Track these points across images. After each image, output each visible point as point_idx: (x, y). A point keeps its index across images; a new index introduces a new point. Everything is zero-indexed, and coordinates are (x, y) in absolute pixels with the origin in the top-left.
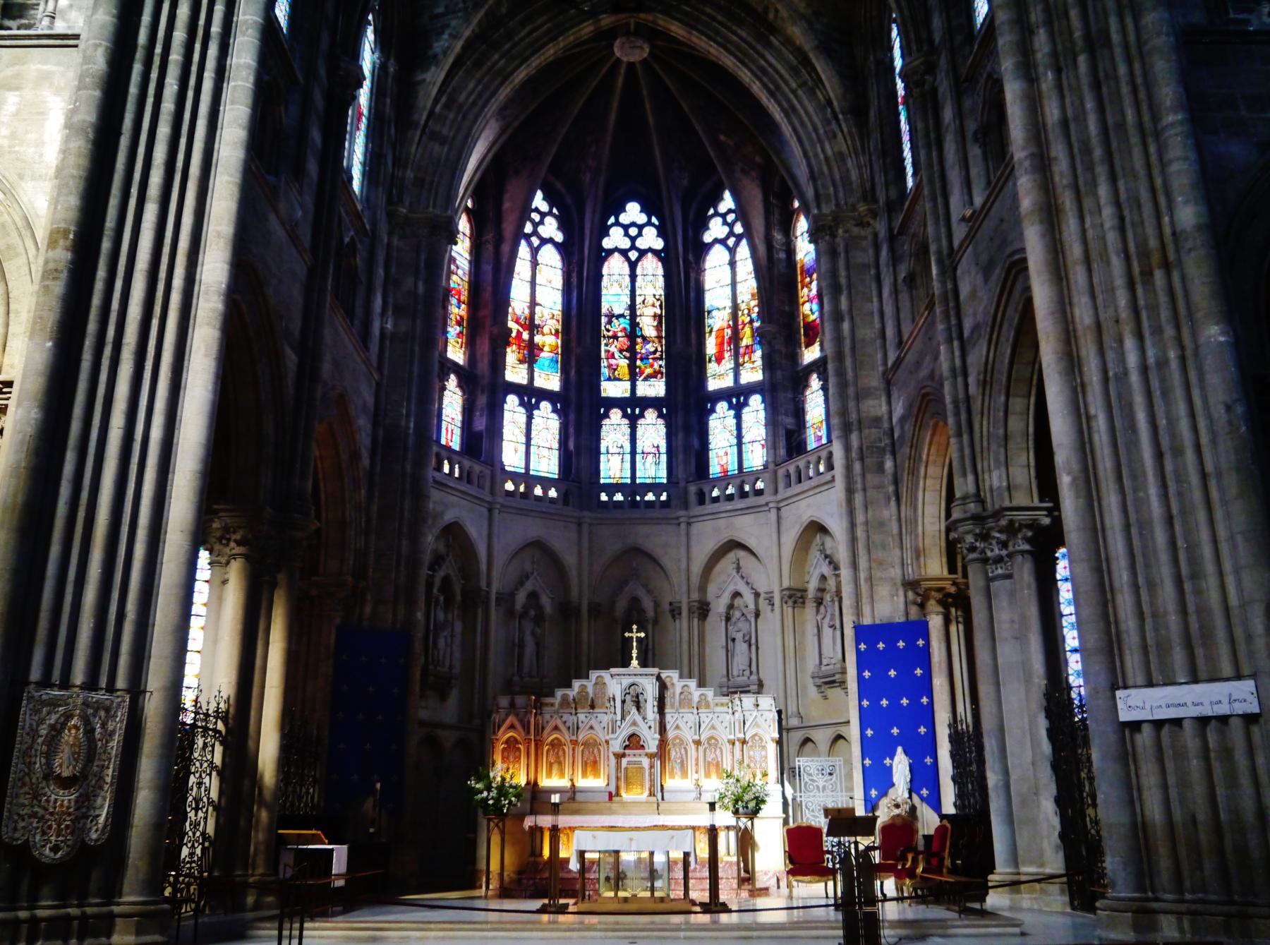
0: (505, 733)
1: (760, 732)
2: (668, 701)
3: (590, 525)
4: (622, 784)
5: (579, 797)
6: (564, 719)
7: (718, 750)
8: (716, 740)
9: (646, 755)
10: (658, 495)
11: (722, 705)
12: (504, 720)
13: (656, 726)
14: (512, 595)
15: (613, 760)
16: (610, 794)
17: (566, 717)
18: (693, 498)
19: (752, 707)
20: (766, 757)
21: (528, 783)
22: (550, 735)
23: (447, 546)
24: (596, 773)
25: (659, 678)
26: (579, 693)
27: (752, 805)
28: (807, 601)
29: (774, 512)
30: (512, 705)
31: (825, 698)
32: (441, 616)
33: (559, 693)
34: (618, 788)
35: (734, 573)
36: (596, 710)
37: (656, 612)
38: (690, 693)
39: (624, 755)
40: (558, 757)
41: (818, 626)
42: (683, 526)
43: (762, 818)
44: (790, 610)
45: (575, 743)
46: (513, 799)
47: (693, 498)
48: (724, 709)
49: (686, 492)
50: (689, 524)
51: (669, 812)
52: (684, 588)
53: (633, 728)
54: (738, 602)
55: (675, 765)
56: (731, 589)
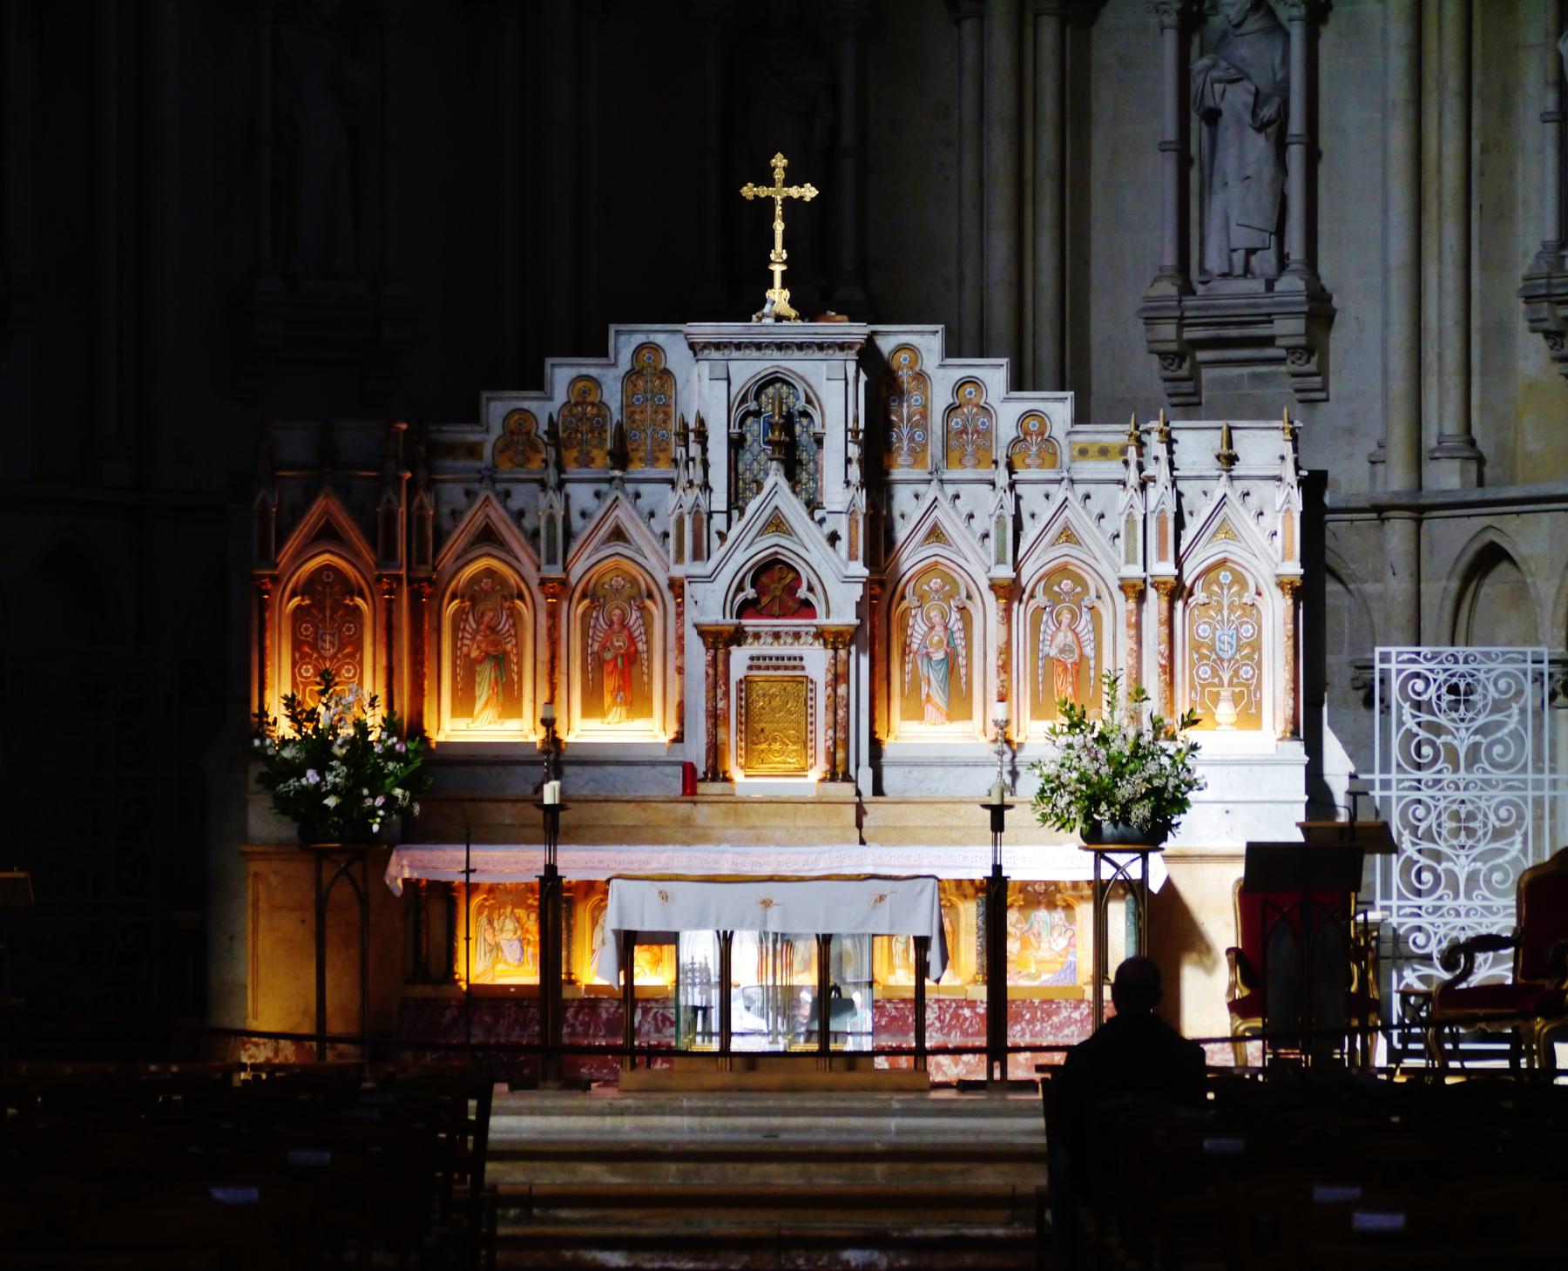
0: (300, 557)
1: (1235, 552)
2: (902, 437)
4: (732, 737)
6: (516, 503)
7: (1086, 617)
8: (1079, 581)
9: (820, 634)
11: (1104, 452)
12: (298, 512)
17: (522, 496)
19: (1210, 465)
20: (1256, 646)
22: (463, 559)
24: (635, 697)
25: (869, 356)
27: (1141, 812)
33: (497, 409)
34: (715, 751)
36: (638, 470)
38: (985, 410)
43: (1231, 857)
45: (559, 589)
46: (398, 792)
48: (1113, 468)
51: (903, 836)
53: (771, 540)
55: (923, 669)
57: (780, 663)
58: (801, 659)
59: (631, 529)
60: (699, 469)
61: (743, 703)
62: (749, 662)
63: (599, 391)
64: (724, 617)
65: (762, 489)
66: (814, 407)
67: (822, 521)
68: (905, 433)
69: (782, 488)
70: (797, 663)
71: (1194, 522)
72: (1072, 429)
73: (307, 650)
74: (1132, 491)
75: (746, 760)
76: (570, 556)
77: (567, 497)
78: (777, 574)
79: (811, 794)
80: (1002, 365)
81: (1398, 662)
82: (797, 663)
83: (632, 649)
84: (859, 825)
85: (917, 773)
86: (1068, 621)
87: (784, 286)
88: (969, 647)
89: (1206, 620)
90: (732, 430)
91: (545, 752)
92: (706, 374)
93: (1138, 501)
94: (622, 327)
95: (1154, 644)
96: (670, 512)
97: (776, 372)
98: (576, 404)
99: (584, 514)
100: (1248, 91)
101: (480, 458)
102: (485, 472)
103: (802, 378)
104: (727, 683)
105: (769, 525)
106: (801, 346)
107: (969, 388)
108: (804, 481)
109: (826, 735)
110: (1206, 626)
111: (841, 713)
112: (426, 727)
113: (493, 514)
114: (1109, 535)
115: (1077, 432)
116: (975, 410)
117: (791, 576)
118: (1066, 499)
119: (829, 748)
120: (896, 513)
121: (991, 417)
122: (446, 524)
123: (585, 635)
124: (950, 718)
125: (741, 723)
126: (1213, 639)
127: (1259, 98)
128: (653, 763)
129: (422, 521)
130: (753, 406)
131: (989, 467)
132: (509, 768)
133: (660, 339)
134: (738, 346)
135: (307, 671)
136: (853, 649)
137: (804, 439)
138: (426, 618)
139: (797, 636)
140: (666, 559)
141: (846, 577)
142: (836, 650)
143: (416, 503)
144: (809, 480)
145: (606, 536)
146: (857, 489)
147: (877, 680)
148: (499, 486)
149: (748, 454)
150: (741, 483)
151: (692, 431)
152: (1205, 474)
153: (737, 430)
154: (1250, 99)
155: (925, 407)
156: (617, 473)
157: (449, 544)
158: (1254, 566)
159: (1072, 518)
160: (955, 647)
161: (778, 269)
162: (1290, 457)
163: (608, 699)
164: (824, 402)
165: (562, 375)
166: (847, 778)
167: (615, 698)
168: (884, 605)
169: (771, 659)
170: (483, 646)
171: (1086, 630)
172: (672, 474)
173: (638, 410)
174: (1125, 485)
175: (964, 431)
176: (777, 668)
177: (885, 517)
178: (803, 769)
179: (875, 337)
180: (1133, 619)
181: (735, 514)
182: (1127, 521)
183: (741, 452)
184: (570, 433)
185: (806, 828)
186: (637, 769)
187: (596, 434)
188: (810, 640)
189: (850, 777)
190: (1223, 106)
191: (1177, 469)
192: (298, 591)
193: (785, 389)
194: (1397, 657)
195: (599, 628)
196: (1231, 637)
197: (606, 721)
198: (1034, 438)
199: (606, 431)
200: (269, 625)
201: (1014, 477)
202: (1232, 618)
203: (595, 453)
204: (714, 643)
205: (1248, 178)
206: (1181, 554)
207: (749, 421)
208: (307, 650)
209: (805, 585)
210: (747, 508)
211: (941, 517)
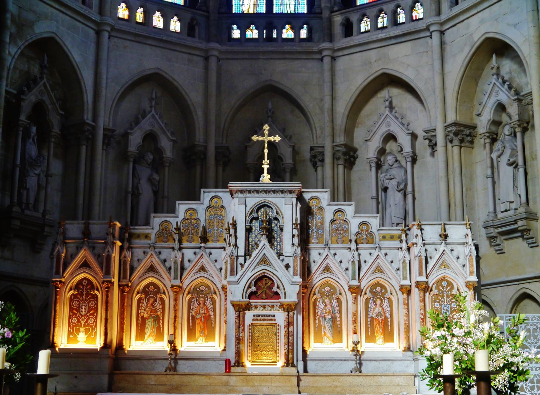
0: (73, 274)
1: (449, 274)
3: (219, 60)
4: (245, 348)
5: (183, 367)
6: (163, 257)
9: (282, 306)
10: (297, 30)
11: (392, 237)
12: (73, 257)
13: (295, 264)
14: (126, 135)
15: (232, 314)
16: (228, 362)
17: (165, 254)
18: (338, 29)
19: (437, 239)
21: (106, 345)
22: (142, 278)
23: (42, 67)
24: (209, 333)
26: (184, 219)
28: (476, 141)
29: (436, 36)
30: (86, 233)
31: (501, 252)
32: (33, 150)
33: (157, 220)
35: (387, 112)
36: (209, 244)
37: (294, 159)
39: (248, 307)
40: (154, 310)
41: (492, 167)
42: (327, 60)
44: (456, 150)
45: (178, 290)
47: (338, 29)
49: (330, 21)
50: (333, 59)
52: (328, 130)
54: (391, 146)
55: (323, 322)
56: (383, 130)
57: (266, 318)
58: (274, 316)
59: (208, 267)
60: (233, 239)
61: (250, 334)
62: (253, 318)
63: (197, 214)
64: (243, 299)
65: (258, 247)
66: (279, 216)
67: (283, 260)
68: (315, 231)
69: (266, 246)
70: (273, 318)
71: (432, 261)
72: (380, 228)
73: (75, 312)
74: (405, 251)
75: (252, 358)
76: (183, 277)
77: (183, 254)
78: (264, 282)
79: (278, 372)
80: (352, 204)
81: (506, 320)
82: (273, 318)
83: (208, 314)
84: (298, 385)
85: (321, 364)
86: (380, 303)
87: (268, 173)
88: (341, 313)
89: (438, 301)
90: (247, 225)
91: (170, 354)
92: (237, 202)
93: (407, 255)
94: (206, 190)
95: (418, 310)
96: (222, 259)
97: (265, 202)
98: (187, 219)
99: (189, 261)
100: (396, 181)
101: (150, 239)
102: (152, 245)
103: (275, 204)
104: (244, 326)
105: (261, 261)
106: (274, 192)
107: (339, 213)
108: (276, 245)
109: (284, 347)
110: (438, 303)
111: (291, 338)
112: (124, 344)
113: (154, 261)
114: (395, 269)
115: (382, 230)
116: (342, 222)
117: (270, 282)
118: (378, 255)
119: (286, 353)
120: (312, 261)
121: (348, 224)
122: (135, 264)
123: (189, 309)
124: (334, 342)
125: (250, 339)
126: (441, 308)
127: (399, 184)
128: (214, 360)
129: (125, 262)
130: (255, 215)
131: (348, 243)
132: (157, 361)
133: (220, 194)
134: (250, 192)
135: (75, 320)
136: (296, 312)
137: (276, 229)
138: (126, 301)
139: (272, 307)
140: (221, 278)
141: (293, 282)
142: (288, 312)
143: (123, 255)
144: (277, 245)
145: (197, 270)
146: (297, 247)
147: (305, 326)
148: (157, 250)
149: (253, 234)
150: (250, 246)
151: (231, 224)
152: (436, 242)
153: (249, 224)
154: (397, 183)
155: (322, 220)
156: (203, 245)
157: (136, 272)
158: (456, 279)
159: (381, 263)
160: (335, 314)
161: (266, 167)
162: (470, 235)
163: (198, 334)
164: (284, 214)
165: (182, 208)
166: (293, 365)
167: (201, 334)
168: (307, 297)
169: (262, 316)
170: (149, 313)
171: (387, 307)
172: (224, 245)
173: (212, 221)
174: (401, 248)
175: (338, 230)
176: (264, 320)
177: (308, 261)
178: (275, 362)
179: (303, 194)
180: (406, 302)
181: (248, 257)
182: (403, 263)
183: (250, 234)
184: (185, 230)
185: (276, 387)
186: (208, 362)
187: (195, 231)
188: (278, 308)
189: (294, 365)
190: (389, 186)
191: (425, 240)
192: (73, 288)
193: (268, 210)
194: (506, 318)
195: (195, 305)
196: (448, 307)
197: (196, 342)
198: (365, 232)
199: (199, 229)
200: (58, 301)
201: (357, 246)
202: (448, 300)
203: (195, 238)
204: (238, 309)
205: (397, 204)
206: (428, 273)
207: (254, 221)
208: (75, 312)
209: (276, 286)
210: (252, 254)
211: (329, 262)
